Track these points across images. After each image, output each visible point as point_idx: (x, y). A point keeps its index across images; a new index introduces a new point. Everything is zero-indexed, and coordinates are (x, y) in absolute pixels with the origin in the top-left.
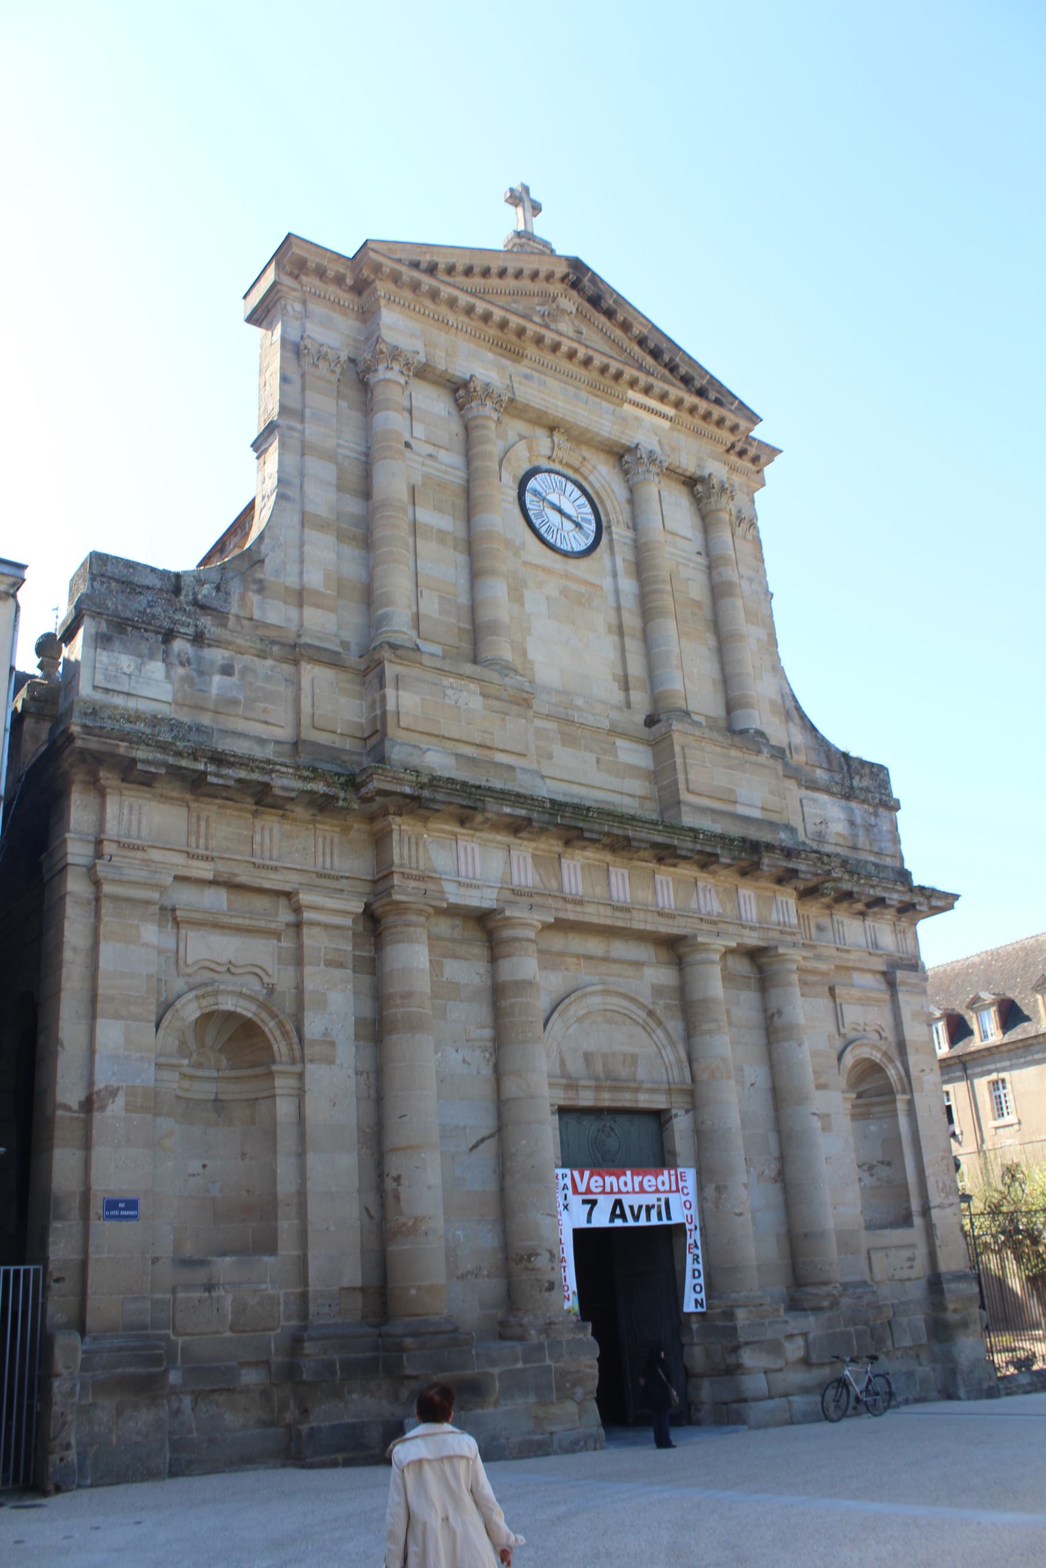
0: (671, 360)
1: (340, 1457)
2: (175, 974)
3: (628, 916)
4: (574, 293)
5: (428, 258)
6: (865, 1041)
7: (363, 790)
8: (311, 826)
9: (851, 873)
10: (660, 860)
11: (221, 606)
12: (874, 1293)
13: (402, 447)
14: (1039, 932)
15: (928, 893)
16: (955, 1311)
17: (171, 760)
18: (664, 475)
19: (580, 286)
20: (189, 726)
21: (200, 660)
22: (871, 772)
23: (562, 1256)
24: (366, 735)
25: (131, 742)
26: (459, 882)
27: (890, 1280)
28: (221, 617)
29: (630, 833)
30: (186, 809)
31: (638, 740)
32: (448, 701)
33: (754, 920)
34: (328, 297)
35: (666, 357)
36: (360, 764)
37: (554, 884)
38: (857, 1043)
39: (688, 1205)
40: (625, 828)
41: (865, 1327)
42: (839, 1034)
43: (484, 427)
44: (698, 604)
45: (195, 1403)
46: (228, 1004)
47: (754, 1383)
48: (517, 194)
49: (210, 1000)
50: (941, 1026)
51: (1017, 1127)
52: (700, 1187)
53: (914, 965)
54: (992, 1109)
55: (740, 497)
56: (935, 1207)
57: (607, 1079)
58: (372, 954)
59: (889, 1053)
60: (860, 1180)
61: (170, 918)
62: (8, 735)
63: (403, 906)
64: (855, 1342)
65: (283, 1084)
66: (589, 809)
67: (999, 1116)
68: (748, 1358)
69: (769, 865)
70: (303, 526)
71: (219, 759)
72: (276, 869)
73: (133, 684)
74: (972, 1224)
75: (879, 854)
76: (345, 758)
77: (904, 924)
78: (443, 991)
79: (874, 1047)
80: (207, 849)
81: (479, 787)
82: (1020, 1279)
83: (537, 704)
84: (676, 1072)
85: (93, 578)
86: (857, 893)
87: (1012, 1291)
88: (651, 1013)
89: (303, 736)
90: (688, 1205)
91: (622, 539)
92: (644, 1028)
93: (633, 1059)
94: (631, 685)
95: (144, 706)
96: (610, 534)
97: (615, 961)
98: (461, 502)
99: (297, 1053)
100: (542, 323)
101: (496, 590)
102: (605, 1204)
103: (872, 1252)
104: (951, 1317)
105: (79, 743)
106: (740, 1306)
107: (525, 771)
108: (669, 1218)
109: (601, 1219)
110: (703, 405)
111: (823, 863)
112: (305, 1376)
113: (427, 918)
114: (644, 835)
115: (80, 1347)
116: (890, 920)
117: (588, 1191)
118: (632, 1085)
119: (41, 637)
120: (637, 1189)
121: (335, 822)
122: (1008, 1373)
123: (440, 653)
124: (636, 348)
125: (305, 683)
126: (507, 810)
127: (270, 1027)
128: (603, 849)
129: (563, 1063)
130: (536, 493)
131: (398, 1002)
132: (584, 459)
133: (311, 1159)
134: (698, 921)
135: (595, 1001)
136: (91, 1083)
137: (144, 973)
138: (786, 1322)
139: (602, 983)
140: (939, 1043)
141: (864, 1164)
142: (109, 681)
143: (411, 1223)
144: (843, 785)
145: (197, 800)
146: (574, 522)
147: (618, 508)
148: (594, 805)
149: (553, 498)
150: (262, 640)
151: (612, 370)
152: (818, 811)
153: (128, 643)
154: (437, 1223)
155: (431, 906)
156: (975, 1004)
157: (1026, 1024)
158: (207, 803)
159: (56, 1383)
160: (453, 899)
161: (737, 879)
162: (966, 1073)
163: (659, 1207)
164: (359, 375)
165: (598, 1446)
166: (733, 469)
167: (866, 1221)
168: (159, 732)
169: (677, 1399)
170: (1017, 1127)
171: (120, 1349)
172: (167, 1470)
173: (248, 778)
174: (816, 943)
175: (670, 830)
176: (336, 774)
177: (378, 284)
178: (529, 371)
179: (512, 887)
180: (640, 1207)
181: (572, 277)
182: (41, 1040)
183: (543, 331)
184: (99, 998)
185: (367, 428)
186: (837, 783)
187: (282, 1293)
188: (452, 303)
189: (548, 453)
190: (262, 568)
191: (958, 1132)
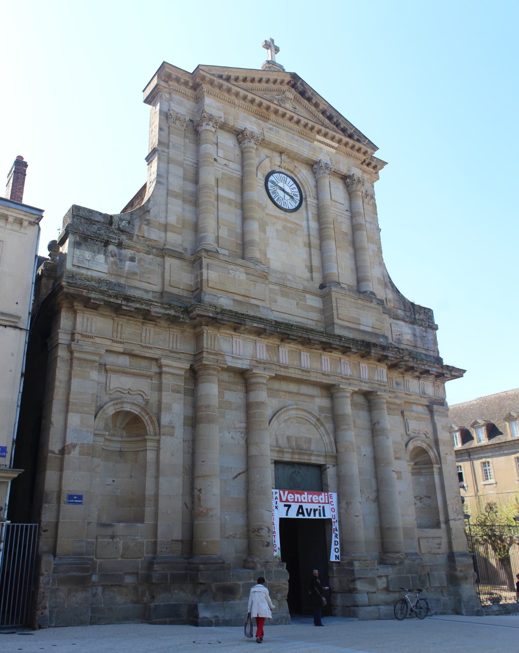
0: (337, 121)
1: (168, 620)
2: (105, 393)
3: (308, 374)
4: (293, 90)
5: (226, 73)
6: (419, 438)
7: (191, 314)
8: (168, 329)
9: (413, 358)
10: (324, 349)
11: (130, 231)
12: (421, 559)
13: (213, 161)
14: (508, 390)
15: (450, 369)
16: (461, 571)
17: (106, 298)
18: (332, 174)
19: (295, 87)
20: (115, 284)
21: (120, 254)
22: (425, 312)
23: (274, 530)
24: (193, 290)
25: (89, 290)
26: (233, 356)
27: (429, 553)
28: (130, 236)
29: (311, 337)
30: (112, 320)
31: (316, 295)
32: (230, 276)
33: (367, 378)
34: (181, 91)
35: (335, 120)
36: (190, 302)
37: (275, 359)
38: (415, 439)
39: (333, 510)
41: (416, 575)
42: (407, 434)
43: (250, 152)
44: (346, 234)
45: (103, 590)
46: (127, 408)
47: (362, 598)
48: (268, 43)
49: (120, 406)
50: (458, 435)
51: (495, 485)
52: (339, 502)
53: (442, 403)
54: (483, 476)
55: (367, 184)
56: (451, 520)
57: (297, 449)
58: (193, 388)
59: (431, 445)
60: (415, 504)
61: (104, 369)
62: (34, 285)
63: (207, 366)
64: (411, 582)
65: (150, 445)
66: (292, 325)
67: (486, 479)
68: (359, 585)
69: (374, 353)
70: (168, 196)
71: (128, 299)
72: (151, 348)
74: (470, 530)
75: (427, 350)
76: (184, 300)
78: (224, 405)
79: (423, 441)
80: (121, 338)
81: (243, 314)
82: (496, 560)
83: (270, 278)
84: (329, 447)
85: (74, 217)
86: (416, 367)
87: (491, 565)
88: (318, 420)
89: (165, 290)
90: (333, 510)
91: (312, 204)
92: (315, 426)
93: (310, 440)
94: (313, 270)
95: (95, 274)
96: (306, 201)
97: (302, 395)
98: (239, 186)
99: (157, 431)
100: (278, 104)
101: (254, 226)
102: (295, 507)
103: (420, 539)
104: (459, 574)
105: (65, 290)
106: (356, 560)
107: (264, 307)
108: (324, 516)
109: (292, 514)
110: (351, 142)
111: (400, 353)
112: (154, 581)
113: (218, 373)
114: (317, 338)
115: (53, 562)
116: (432, 380)
117: (287, 501)
118: (308, 452)
120: (310, 501)
121: (178, 328)
122: (487, 604)
123: (228, 254)
124: (321, 115)
125: (167, 266)
126: (255, 325)
127: (146, 419)
128: (298, 344)
129: (277, 441)
130: (273, 182)
131: (203, 409)
132: (295, 167)
133: (162, 480)
135: (293, 413)
136: (64, 441)
137: (91, 393)
138: (378, 570)
139: (297, 405)
140: (457, 442)
141: (417, 496)
143: (205, 511)
144: (411, 317)
146: (290, 196)
147: (310, 190)
148: (295, 324)
149: (281, 184)
150: (148, 246)
151: (310, 126)
152: (399, 329)
154: (217, 512)
155: (220, 367)
157: (500, 436)
158: (122, 318)
159: (41, 578)
160: (230, 364)
162: (470, 457)
163: (320, 510)
164: (194, 128)
165: (287, 623)
166: (364, 171)
167: (418, 524)
168: (101, 286)
169: (325, 603)
170: (495, 485)
171: (71, 564)
174: (395, 390)
175: (329, 336)
177: (204, 85)
178: (271, 126)
179: (256, 360)
180: (311, 509)
181: (292, 82)
183: (278, 108)
184: (70, 403)
185: (197, 152)
186: (408, 317)
187: (145, 541)
188: (237, 94)
189: (279, 164)
190: (149, 214)
191: (465, 485)
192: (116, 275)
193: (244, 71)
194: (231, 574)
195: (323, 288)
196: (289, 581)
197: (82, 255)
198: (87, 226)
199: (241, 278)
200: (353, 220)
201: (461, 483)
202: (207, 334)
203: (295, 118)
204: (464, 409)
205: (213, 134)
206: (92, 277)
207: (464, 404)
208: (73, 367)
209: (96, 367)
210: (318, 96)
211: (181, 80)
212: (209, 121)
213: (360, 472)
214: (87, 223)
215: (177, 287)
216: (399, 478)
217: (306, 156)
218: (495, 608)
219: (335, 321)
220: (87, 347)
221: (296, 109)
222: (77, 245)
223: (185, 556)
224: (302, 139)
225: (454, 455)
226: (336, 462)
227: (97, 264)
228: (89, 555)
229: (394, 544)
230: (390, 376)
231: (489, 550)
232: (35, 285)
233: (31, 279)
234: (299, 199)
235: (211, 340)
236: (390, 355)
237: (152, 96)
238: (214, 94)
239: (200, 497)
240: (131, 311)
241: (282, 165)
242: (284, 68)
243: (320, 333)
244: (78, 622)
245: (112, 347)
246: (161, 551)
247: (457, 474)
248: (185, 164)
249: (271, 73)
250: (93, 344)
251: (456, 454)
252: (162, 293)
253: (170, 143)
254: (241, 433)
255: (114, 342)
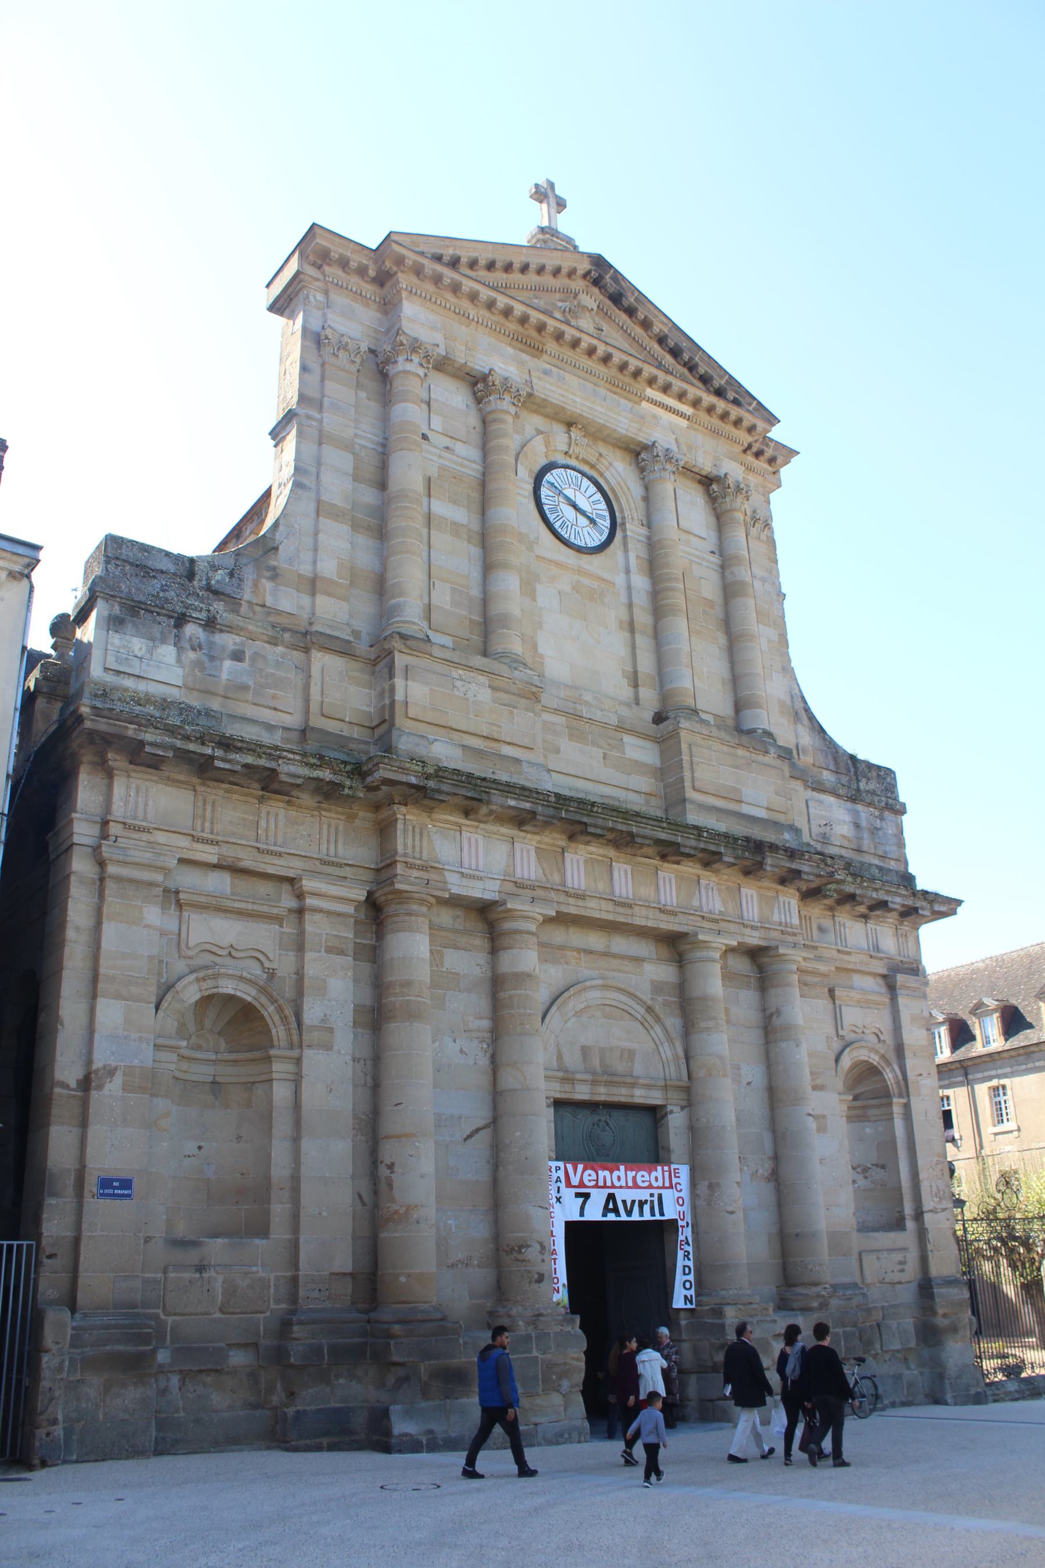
0: (691, 359)
1: (325, 1441)
2: (177, 956)
3: (629, 911)
4: (596, 290)
5: (451, 251)
6: (863, 1044)
7: (369, 779)
8: (316, 813)
9: (854, 875)
10: (663, 857)
12: (864, 1295)
13: (419, 439)
16: (945, 1316)
17: (179, 743)
18: (680, 473)
19: (601, 284)
20: (198, 711)
21: (211, 645)
22: (879, 775)
23: (553, 1248)
24: (374, 724)
26: (462, 873)
28: (233, 602)
29: (634, 830)
31: (646, 737)
32: (456, 693)
33: (756, 919)
34: (350, 288)
35: (686, 356)
36: (367, 752)
38: (856, 1045)
40: (629, 824)
41: (854, 1329)
42: (838, 1036)
43: (502, 421)
44: (710, 603)
45: (183, 1382)
46: (228, 987)
48: (543, 190)
49: (210, 983)
50: (944, 1031)
51: (1016, 1134)
52: (693, 1184)
53: (915, 969)
54: (992, 1115)
55: (756, 497)
57: (604, 1073)
58: (373, 943)
59: (887, 1057)
60: (854, 1181)
61: (174, 901)
62: (18, 714)
63: (405, 895)
64: (843, 1343)
66: (593, 804)
67: (999, 1123)
69: (772, 866)
70: (318, 514)
71: (227, 744)
72: (280, 855)
73: (144, 667)
74: (965, 1230)
75: (883, 857)
76: (353, 746)
77: (906, 928)
78: (444, 981)
79: (872, 1049)
80: (212, 833)
81: (484, 779)
82: (1015, 1286)
84: (673, 1068)
86: (860, 895)
87: (1006, 1296)
88: (649, 1009)
89: (311, 724)
91: (636, 536)
93: (631, 1054)
94: (640, 683)
95: (154, 689)
96: (624, 530)
97: (615, 956)
98: (476, 495)
99: (295, 1038)
100: (563, 319)
101: (509, 583)
102: (598, 1198)
104: (940, 1321)
105: (88, 724)
106: (728, 1304)
108: (662, 1214)
109: (594, 1213)
110: (721, 405)
111: (826, 865)
112: (292, 1360)
114: (647, 832)
115: (70, 1324)
116: (892, 923)
117: (581, 1184)
118: (629, 1080)
119: (56, 618)
120: (630, 1184)
121: (340, 809)
122: (996, 1379)
123: (451, 645)
124: (656, 346)
125: (315, 671)
126: (512, 803)
127: (269, 1011)
128: (606, 845)
129: (560, 1057)
131: (397, 991)
132: (601, 455)
133: (306, 1144)
134: (700, 919)
135: (595, 995)
136: (89, 1062)
137: (146, 954)
138: (775, 1321)
139: (602, 978)
140: (941, 1047)
141: (859, 1166)
142: (120, 664)
143: (402, 1211)
144: (849, 787)
145: (203, 784)
146: (588, 518)
148: (600, 800)
149: (569, 493)
151: (631, 368)
152: (824, 813)
153: (141, 627)
154: (429, 1212)
155: (433, 896)
156: (978, 1010)
157: (1028, 1031)
158: (214, 788)
159: (45, 1359)
160: (455, 890)
161: (740, 879)
163: (652, 1202)
165: (583, 1439)
166: (749, 469)
168: (169, 715)
170: (1016, 1134)
171: (108, 1327)
172: (153, 1449)
173: (255, 763)
175: (674, 827)
176: (343, 762)
178: (548, 366)
179: (514, 880)
180: (633, 1202)
182: (42, 1018)
184: (101, 978)
185: (385, 419)
186: (843, 785)
187: (272, 1276)
188: (473, 297)
189: (565, 448)
190: (276, 555)
191: (957, 1137)
192: (201, 691)
193: (490, 246)
194: (461, 1341)
195: (662, 722)
196: (585, 1353)
197: (124, 647)
198: (137, 581)
199: (480, 697)
200: (726, 574)
201: (949, 1133)
202: (405, 824)
203: (599, 351)
204: (960, 980)
205: (419, 381)
206: (147, 695)
207: (959, 969)
208: (106, 898)
209: (155, 896)
210: (649, 305)
211: (351, 263)
212: (411, 353)
213: (738, 1120)
214: (137, 575)
215: (338, 717)
216: (822, 1129)
217: (624, 432)
218: (1012, 1386)
219: (687, 795)
220: (137, 853)
221: (602, 330)
222: (114, 625)
223: (360, 1306)
224: (616, 397)
225: (935, 1076)
226: (688, 1100)
227: (158, 667)
228: (149, 1308)
229: (810, 1267)
230: (806, 913)
231: (1002, 1269)
232: (21, 714)
233: (12, 700)
234: (609, 525)
235: (414, 836)
236: (805, 868)
237: (285, 297)
238: (423, 295)
239: (392, 1181)
240: (235, 772)
241: (571, 449)
242: (577, 244)
243: (655, 820)
244: (127, 1450)
245: (192, 852)
246: (308, 1298)
247: (941, 1115)
248: (357, 447)
249: (548, 253)
250: (149, 845)
251: (939, 1072)
252: (303, 731)
253: (326, 399)
254: (480, 1042)
255: (198, 841)
